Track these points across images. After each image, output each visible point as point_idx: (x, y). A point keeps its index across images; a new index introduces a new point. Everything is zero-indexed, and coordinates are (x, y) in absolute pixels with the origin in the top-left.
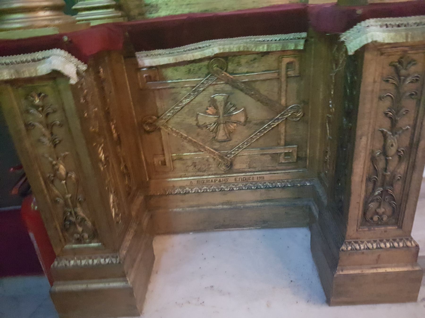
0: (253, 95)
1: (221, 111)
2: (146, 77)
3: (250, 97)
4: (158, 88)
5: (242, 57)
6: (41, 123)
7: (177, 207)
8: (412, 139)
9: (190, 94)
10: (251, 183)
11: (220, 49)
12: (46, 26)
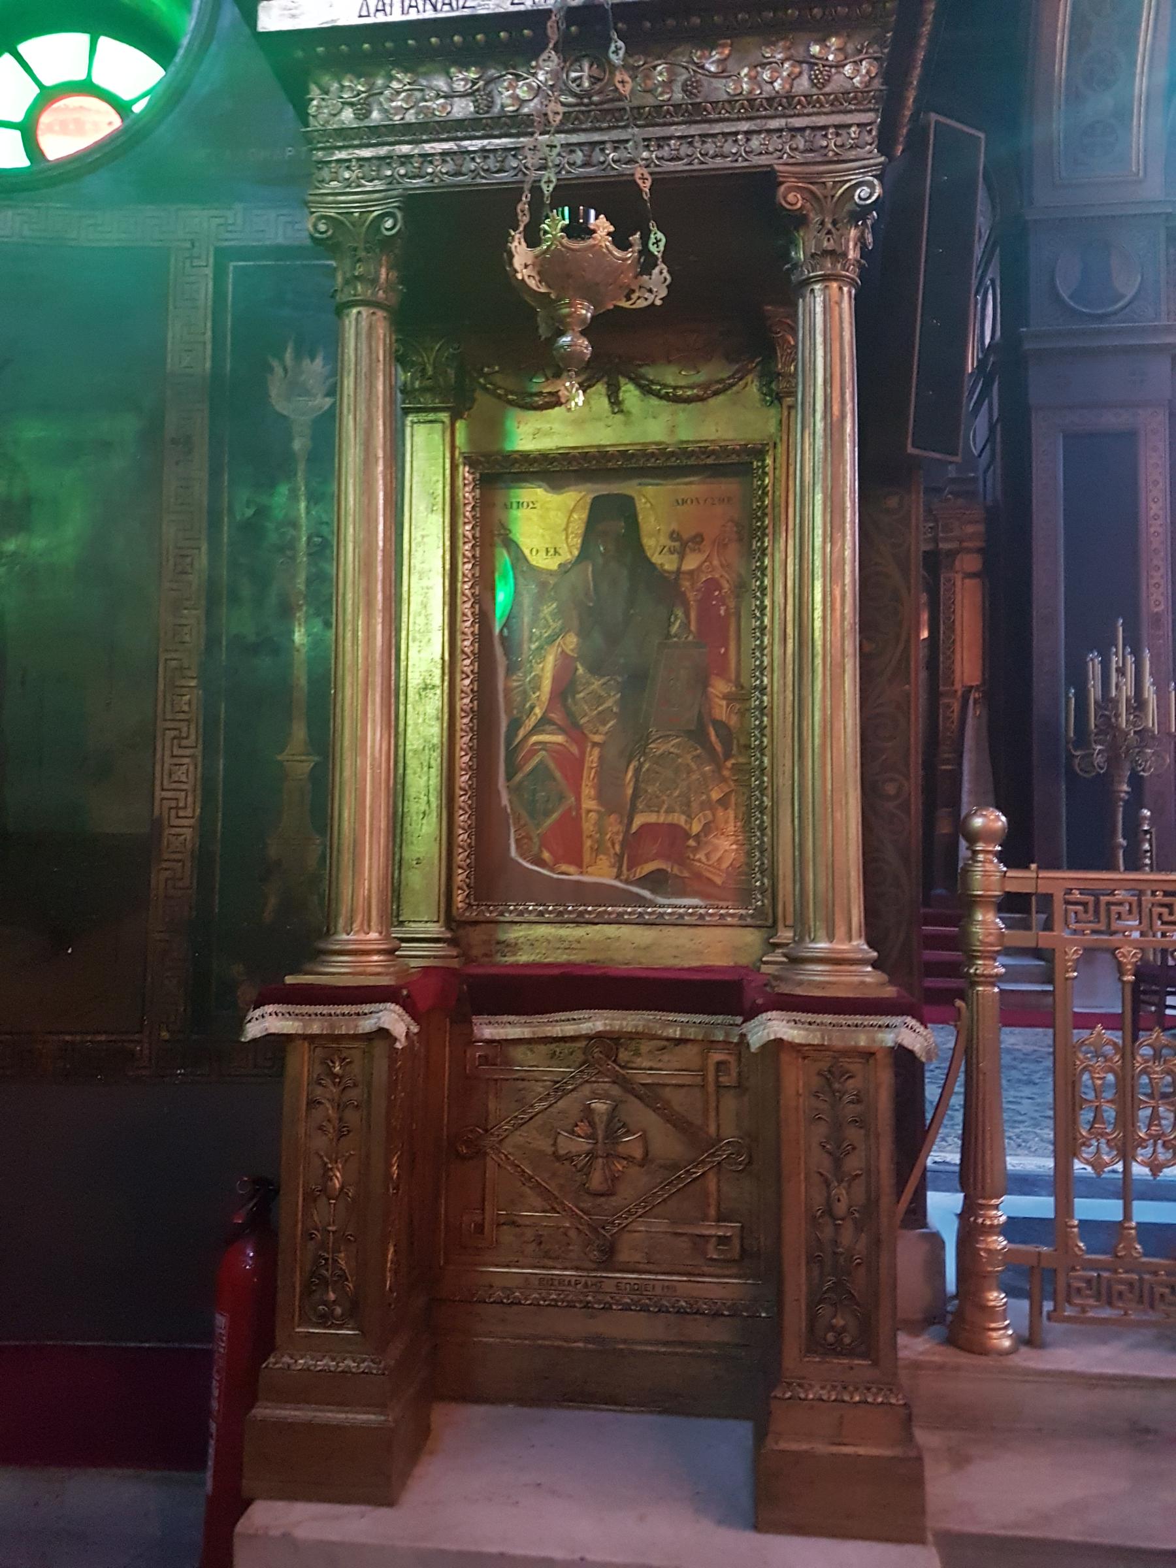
0: (659, 1108)
1: (600, 1134)
2: (480, 1056)
3: (653, 1114)
4: (496, 1077)
5: (643, 1041)
6: (331, 1101)
7: (490, 1334)
8: (868, 1191)
9: (548, 1094)
10: (650, 1299)
11: (605, 1025)
12: (378, 974)
